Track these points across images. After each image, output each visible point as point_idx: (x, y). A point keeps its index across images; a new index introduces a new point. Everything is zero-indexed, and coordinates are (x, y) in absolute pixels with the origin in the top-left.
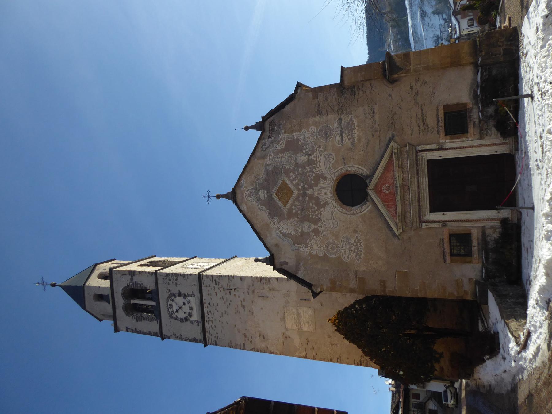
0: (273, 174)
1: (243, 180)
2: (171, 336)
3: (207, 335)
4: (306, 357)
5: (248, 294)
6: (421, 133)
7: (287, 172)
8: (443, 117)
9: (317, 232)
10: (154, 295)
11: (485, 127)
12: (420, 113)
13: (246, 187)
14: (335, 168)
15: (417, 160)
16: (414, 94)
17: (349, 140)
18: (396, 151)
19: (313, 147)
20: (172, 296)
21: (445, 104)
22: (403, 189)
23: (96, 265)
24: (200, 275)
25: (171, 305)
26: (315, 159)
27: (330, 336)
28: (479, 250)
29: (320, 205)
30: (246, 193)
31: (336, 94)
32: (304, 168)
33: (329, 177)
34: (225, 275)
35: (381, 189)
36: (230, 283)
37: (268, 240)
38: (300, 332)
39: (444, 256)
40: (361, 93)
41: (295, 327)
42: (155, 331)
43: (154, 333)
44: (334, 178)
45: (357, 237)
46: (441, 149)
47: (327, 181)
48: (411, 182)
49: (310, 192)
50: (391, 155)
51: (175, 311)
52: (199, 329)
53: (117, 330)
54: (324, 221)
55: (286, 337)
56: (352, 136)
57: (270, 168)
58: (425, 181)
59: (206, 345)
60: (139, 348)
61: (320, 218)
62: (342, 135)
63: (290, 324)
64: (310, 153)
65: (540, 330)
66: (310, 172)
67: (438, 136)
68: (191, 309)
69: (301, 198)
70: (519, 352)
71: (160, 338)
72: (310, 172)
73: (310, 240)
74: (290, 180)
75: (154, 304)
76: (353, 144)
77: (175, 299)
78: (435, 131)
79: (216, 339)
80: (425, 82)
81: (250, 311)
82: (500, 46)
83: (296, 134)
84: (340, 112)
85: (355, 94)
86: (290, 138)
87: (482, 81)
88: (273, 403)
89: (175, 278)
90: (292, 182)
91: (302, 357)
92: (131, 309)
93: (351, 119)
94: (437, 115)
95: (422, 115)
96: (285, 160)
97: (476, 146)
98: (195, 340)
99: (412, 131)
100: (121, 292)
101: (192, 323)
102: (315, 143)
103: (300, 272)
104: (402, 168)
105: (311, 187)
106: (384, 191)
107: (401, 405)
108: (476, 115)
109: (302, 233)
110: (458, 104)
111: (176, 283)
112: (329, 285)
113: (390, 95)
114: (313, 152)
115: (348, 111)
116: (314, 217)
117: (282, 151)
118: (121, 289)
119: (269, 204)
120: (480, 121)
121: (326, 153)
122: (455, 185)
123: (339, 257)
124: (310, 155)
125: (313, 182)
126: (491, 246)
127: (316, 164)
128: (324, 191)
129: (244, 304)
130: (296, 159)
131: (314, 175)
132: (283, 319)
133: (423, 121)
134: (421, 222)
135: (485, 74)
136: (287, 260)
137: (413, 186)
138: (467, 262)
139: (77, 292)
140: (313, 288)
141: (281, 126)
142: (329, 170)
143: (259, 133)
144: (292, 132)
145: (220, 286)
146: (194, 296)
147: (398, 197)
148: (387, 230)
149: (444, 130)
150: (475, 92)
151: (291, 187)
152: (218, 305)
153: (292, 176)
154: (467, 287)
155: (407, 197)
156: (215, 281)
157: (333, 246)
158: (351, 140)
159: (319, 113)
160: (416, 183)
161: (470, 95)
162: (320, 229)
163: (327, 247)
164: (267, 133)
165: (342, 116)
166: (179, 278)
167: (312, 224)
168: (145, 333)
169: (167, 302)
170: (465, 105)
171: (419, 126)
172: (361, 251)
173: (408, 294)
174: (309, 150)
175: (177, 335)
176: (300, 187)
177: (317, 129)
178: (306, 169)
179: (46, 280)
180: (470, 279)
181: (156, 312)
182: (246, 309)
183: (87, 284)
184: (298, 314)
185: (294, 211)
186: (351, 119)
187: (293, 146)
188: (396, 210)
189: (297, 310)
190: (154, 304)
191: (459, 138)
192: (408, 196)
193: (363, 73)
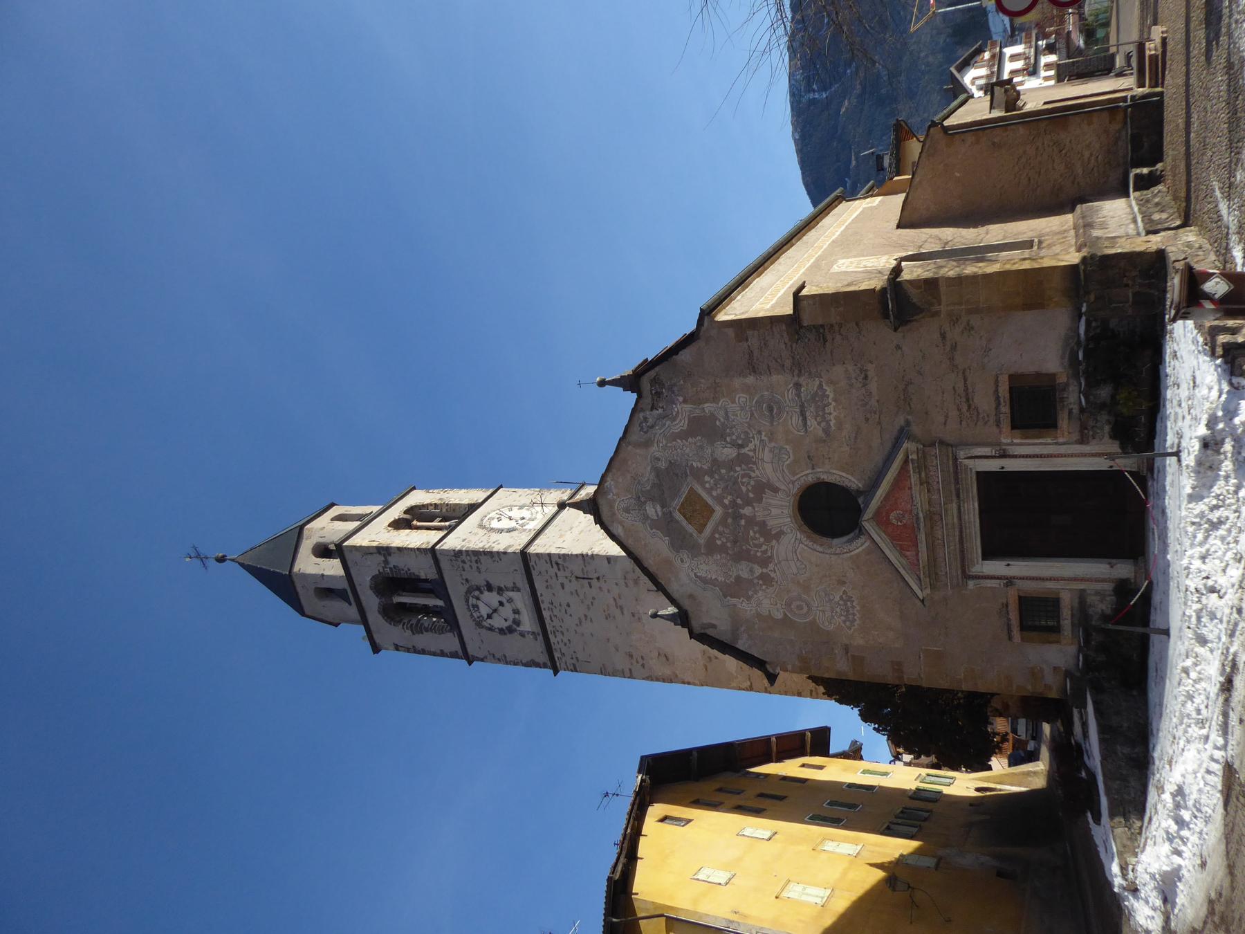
0: (668, 478)
3: (557, 655)
4: (751, 689)
6: (964, 423)
7: (698, 474)
8: (1007, 395)
9: (766, 579)
10: (437, 587)
11: (1091, 423)
12: (961, 385)
14: (794, 474)
15: (956, 473)
16: (948, 348)
17: (819, 424)
18: (914, 457)
19: (746, 433)
20: (473, 590)
21: (1012, 372)
23: (301, 528)
24: (524, 554)
25: (476, 607)
26: (751, 454)
28: (1073, 625)
30: (619, 505)
31: (785, 335)
32: (731, 469)
33: (783, 487)
34: (575, 553)
37: (674, 588)
39: (1009, 631)
40: (838, 337)
42: (453, 649)
45: (845, 593)
46: (1004, 455)
48: (946, 510)
49: (747, 511)
50: (906, 461)
52: (539, 645)
54: (779, 562)
57: (663, 465)
58: (972, 508)
59: (556, 672)
60: (424, 679)
61: (771, 557)
62: (803, 414)
64: (740, 442)
66: (743, 476)
67: (996, 430)
68: (516, 612)
69: (730, 520)
71: (464, 662)
72: (743, 476)
74: (705, 488)
75: (440, 603)
76: (827, 431)
77: (482, 596)
78: (992, 419)
80: (969, 328)
82: (1127, 285)
83: (708, 407)
84: (796, 372)
85: (825, 341)
86: (697, 413)
87: (1088, 339)
89: (474, 559)
90: (709, 491)
92: (394, 613)
93: (820, 386)
94: (996, 391)
95: (966, 389)
96: (690, 451)
97: (1072, 456)
98: (533, 664)
99: (947, 417)
100: (368, 584)
102: (750, 426)
104: (928, 483)
105: (748, 502)
106: (894, 521)
108: (1073, 398)
109: (738, 578)
110: (1038, 375)
112: (797, 663)
113: (898, 347)
114: (747, 441)
117: (684, 435)
119: (667, 525)
120: (1082, 410)
121: (773, 444)
122: (1022, 514)
123: (813, 622)
124: (741, 446)
125: (751, 495)
127: (754, 463)
128: (775, 511)
129: (620, 602)
130: (713, 452)
131: (752, 483)
133: (968, 400)
134: (967, 576)
135: (1094, 324)
136: (714, 622)
137: (950, 518)
138: (1050, 643)
139: (284, 585)
142: (781, 473)
143: (635, 396)
144: (699, 402)
146: (519, 590)
147: (922, 537)
149: (1009, 420)
150: (1074, 355)
151: (709, 501)
154: (1051, 679)
155: (939, 534)
159: (754, 370)
160: (955, 512)
161: (1062, 357)
162: (773, 575)
163: (789, 605)
164: (647, 400)
165: (802, 380)
167: (756, 567)
168: (434, 654)
169: (467, 601)
170: (1053, 376)
171: (959, 410)
173: (943, 684)
174: (738, 437)
175: (497, 656)
176: (726, 501)
179: (203, 551)
180: (1055, 668)
183: (296, 569)
185: (719, 542)
186: (820, 386)
187: (703, 428)
190: (440, 603)
193: (841, 309)
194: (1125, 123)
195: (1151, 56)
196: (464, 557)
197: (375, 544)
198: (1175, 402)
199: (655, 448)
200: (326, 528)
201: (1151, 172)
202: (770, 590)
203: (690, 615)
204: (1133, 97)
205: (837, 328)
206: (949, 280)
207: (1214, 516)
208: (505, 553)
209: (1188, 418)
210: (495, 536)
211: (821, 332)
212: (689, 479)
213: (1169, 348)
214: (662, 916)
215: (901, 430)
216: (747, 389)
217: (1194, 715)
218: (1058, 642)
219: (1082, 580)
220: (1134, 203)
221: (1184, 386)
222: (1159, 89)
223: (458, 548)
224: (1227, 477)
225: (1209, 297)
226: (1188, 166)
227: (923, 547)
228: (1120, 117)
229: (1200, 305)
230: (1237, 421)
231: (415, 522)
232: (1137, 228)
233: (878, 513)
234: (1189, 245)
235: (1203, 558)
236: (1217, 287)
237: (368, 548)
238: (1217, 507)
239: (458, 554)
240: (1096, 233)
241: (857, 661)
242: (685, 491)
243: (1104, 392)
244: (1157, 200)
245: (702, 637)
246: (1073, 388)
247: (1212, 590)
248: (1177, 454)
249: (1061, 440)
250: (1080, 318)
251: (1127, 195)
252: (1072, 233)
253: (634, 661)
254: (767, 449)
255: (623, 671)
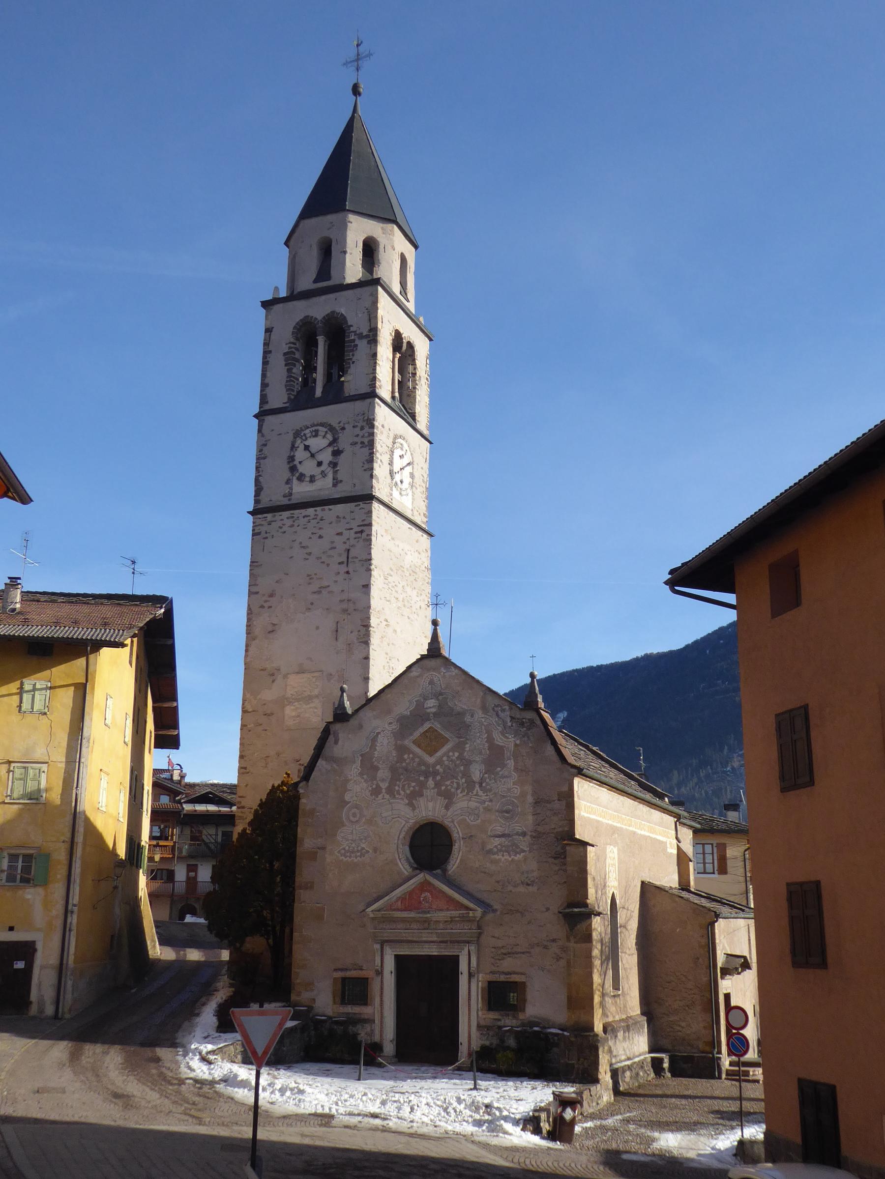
0: (457, 722)
1: (455, 672)
2: (263, 436)
3: (269, 516)
4: (244, 711)
5: (341, 601)
6: (493, 950)
7: (459, 747)
8: (511, 980)
9: (376, 791)
10: (335, 394)
11: (491, 1033)
13: (444, 677)
15: (458, 942)
16: (546, 943)
18: (471, 915)
19: (490, 790)
21: (528, 984)
22: (425, 921)
24: (370, 498)
25: (316, 434)
26: (475, 792)
27: (278, 754)
28: (348, 1013)
29: (413, 797)
31: (561, 829)
33: (449, 813)
34: (373, 551)
35: (426, 891)
36: (355, 559)
38: (283, 702)
39: (341, 970)
41: (290, 692)
42: (270, 398)
43: (266, 395)
44: (447, 823)
45: (368, 852)
46: (470, 975)
47: (443, 810)
49: (431, 783)
50: (468, 908)
51: (307, 443)
52: (279, 499)
53: (266, 304)
54: (390, 803)
55: (273, 675)
56: (501, 851)
57: (468, 719)
59: (251, 513)
60: (235, 372)
61: (394, 797)
63: (296, 684)
65: (207, 1072)
66: (458, 784)
68: (312, 479)
69: (423, 768)
70: (200, 1053)
71: (257, 411)
72: (458, 784)
73: (366, 781)
75: (319, 392)
76: (490, 852)
78: (494, 969)
79: (263, 535)
80: (558, 958)
81: (312, 604)
83: (511, 763)
84: (534, 834)
85: (555, 858)
86: (507, 754)
87: (547, 1034)
88: (170, 642)
89: (366, 440)
90: (446, 754)
91: (243, 704)
92: (307, 333)
94: (515, 973)
95: (517, 953)
96: (478, 742)
100: (337, 310)
101: (288, 482)
102: (495, 794)
103: (324, 763)
104: (451, 921)
105: (437, 785)
106: (423, 895)
107: (225, 809)
108: (509, 1022)
109: (376, 769)
111: (356, 443)
112: (308, 808)
114: (485, 790)
115: (535, 847)
116: (397, 788)
117: (490, 740)
118: (343, 311)
119: (418, 716)
120: (500, 1027)
121: (482, 810)
122: (428, 986)
124: (481, 784)
125: (443, 788)
126: (351, 1029)
127: (468, 794)
128: (431, 804)
129: (324, 592)
131: (453, 790)
132: (301, 671)
134: (383, 943)
136: (340, 743)
138: (334, 997)
140: (304, 783)
141: (526, 739)
142: (460, 814)
145: (352, 542)
146: (335, 485)
148: (375, 895)
150: (537, 1024)
151: (439, 754)
152: (320, 537)
153: (454, 755)
156: (362, 532)
157: (358, 816)
158: (495, 850)
159: (537, 802)
160: (430, 939)
162: (380, 796)
163: (357, 807)
165: (528, 838)
166: (366, 451)
167: (387, 785)
168: (264, 376)
169: (322, 425)
170: (523, 1010)
172: (350, 857)
173: (297, 919)
174: (488, 784)
175: (264, 449)
176: (438, 767)
177: (515, 798)
178: (462, 778)
180: (314, 1000)
181: (303, 398)
182: (316, 596)
183: (351, 217)
184: (310, 699)
185: (406, 756)
188: (398, 910)
189: (317, 697)
190: (319, 392)
191: (482, 998)
192: (415, 927)
194: (703, 1052)
195: (748, 1072)
196: (367, 429)
197: (379, 326)
198: (506, 1087)
199: (480, 712)
200: (395, 246)
201: (664, 1069)
202: (368, 794)
203: (345, 724)
204: (720, 1058)
205: (564, 868)
206: (590, 951)
207: (450, 1110)
208: (372, 476)
209: (498, 1096)
210: (385, 458)
211: (561, 856)
212: (457, 740)
213: (538, 1084)
214: (87, 681)
215: (491, 906)
216: (523, 795)
217: (342, 1098)
218: (335, 1003)
219: (382, 1022)
220: (642, 1057)
221: (516, 1094)
222: (724, 1076)
223: (376, 424)
224: (471, 1116)
225: (564, 1110)
226: (656, 1096)
227: (405, 914)
228: (708, 1049)
229: (560, 1106)
230: (502, 1122)
231: (398, 355)
232: (621, 1061)
233: (429, 884)
234: (600, 1097)
235: (427, 1104)
236: (568, 1114)
237: (376, 317)
238: (455, 1111)
239: (370, 423)
240: (620, 1035)
241: (313, 856)
242: (447, 735)
243: (511, 1042)
244: (641, 1074)
245: (326, 733)
246: (514, 1022)
247: (412, 1109)
248: (475, 1088)
249: (480, 1013)
250: (560, 1029)
251: (650, 1052)
252: (624, 1017)
253: (264, 598)
254: (478, 805)
255: (256, 585)
